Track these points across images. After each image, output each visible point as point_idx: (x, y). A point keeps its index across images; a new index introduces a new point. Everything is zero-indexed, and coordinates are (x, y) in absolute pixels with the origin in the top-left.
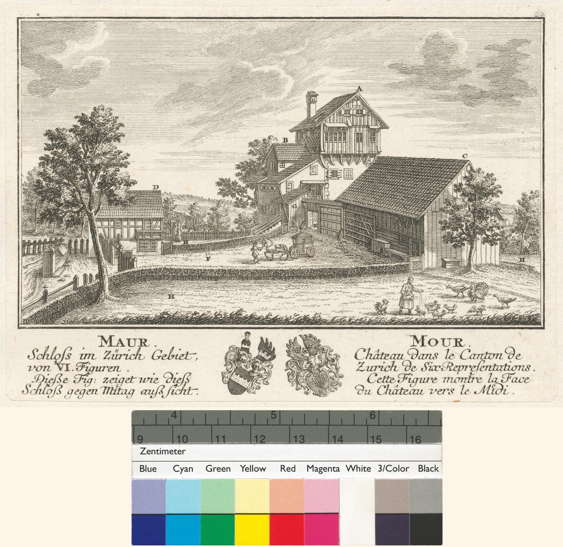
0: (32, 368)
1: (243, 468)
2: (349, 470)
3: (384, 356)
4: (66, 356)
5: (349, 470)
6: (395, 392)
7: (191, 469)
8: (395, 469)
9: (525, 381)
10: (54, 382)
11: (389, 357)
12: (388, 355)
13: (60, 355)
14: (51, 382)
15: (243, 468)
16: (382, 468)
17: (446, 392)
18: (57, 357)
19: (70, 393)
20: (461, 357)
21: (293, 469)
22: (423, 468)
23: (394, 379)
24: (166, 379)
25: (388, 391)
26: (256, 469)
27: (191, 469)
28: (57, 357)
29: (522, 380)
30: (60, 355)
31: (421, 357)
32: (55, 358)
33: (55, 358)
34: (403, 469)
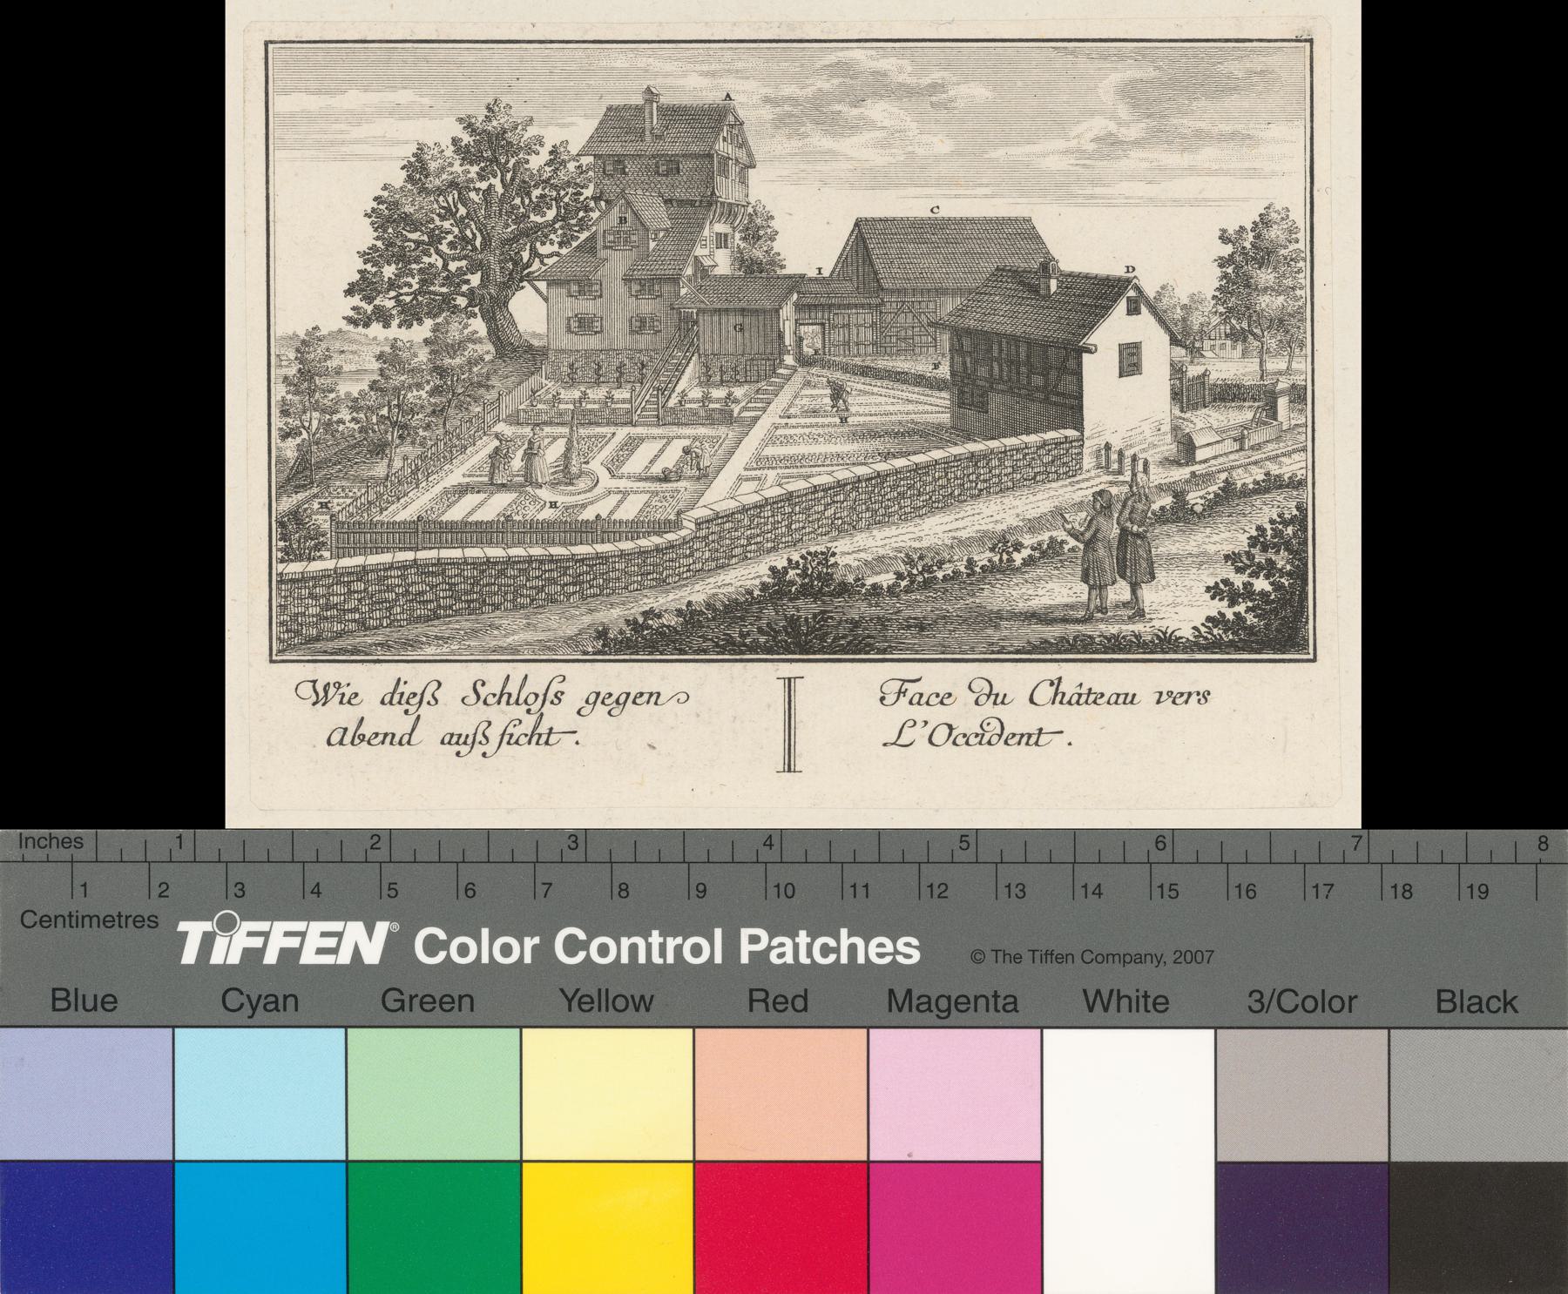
0: (1165, 696)
1: (570, 1001)
2: (1091, 1009)
3: (1092, 697)
4: (551, 696)
5: (1091, 1009)
6: (1075, 698)
7: (291, 1001)
8: (1310, 1004)
9: (942, 703)
10: (421, 702)
11: (1105, 699)
12: (1102, 695)
13: (537, 696)
14: (413, 701)
15: (570, 1001)
16: (1266, 1001)
17: (1194, 698)
18: (531, 699)
19: (592, 699)
20: (1031, 701)
21: (799, 1003)
22: (72, 998)
23: (1102, 695)
24: (975, 696)
25: (1059, 698)
26: (620, 1003)
27: (291, 1001)
28: (531, 699)
29: (934, 700)
30: (537, 696)
31: (915, 700)
32: (526, 702)
33: (526, 702)
34: (1337, 1004)
